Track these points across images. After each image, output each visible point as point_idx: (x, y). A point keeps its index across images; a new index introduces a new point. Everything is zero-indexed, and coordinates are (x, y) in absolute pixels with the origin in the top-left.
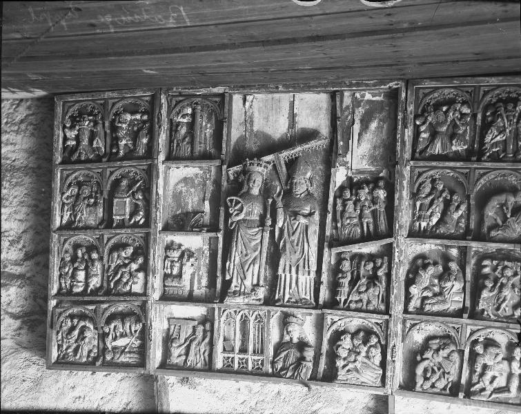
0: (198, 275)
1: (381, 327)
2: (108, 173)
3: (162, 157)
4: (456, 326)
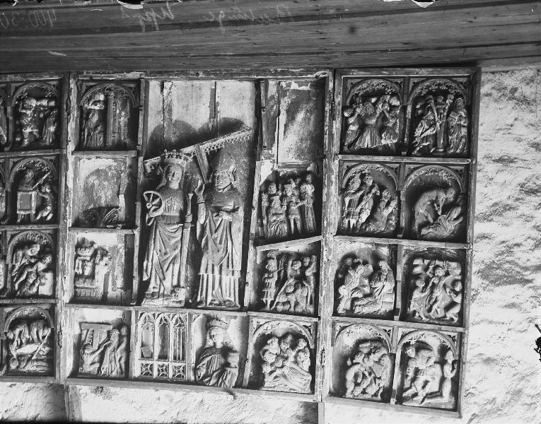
0: (113, 275)
1: (310, 330)
2: (11, 164)
4: (387, 329)
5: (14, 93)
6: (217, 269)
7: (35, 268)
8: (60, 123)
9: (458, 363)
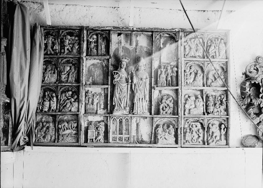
0: (100, 104)
1: (175, 121)
2: (60, 61)
3: (85, 54)
4: (202, 119)
5: (62, 33)
6: (141, 100)
7: (70, 100)
8: (80, 44)
9: (227, 128)
